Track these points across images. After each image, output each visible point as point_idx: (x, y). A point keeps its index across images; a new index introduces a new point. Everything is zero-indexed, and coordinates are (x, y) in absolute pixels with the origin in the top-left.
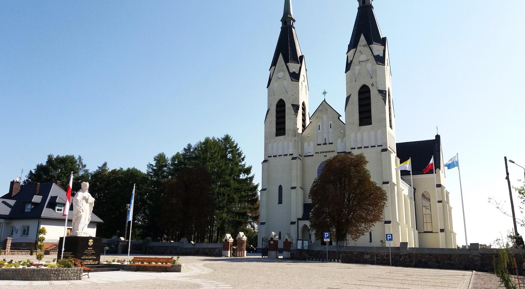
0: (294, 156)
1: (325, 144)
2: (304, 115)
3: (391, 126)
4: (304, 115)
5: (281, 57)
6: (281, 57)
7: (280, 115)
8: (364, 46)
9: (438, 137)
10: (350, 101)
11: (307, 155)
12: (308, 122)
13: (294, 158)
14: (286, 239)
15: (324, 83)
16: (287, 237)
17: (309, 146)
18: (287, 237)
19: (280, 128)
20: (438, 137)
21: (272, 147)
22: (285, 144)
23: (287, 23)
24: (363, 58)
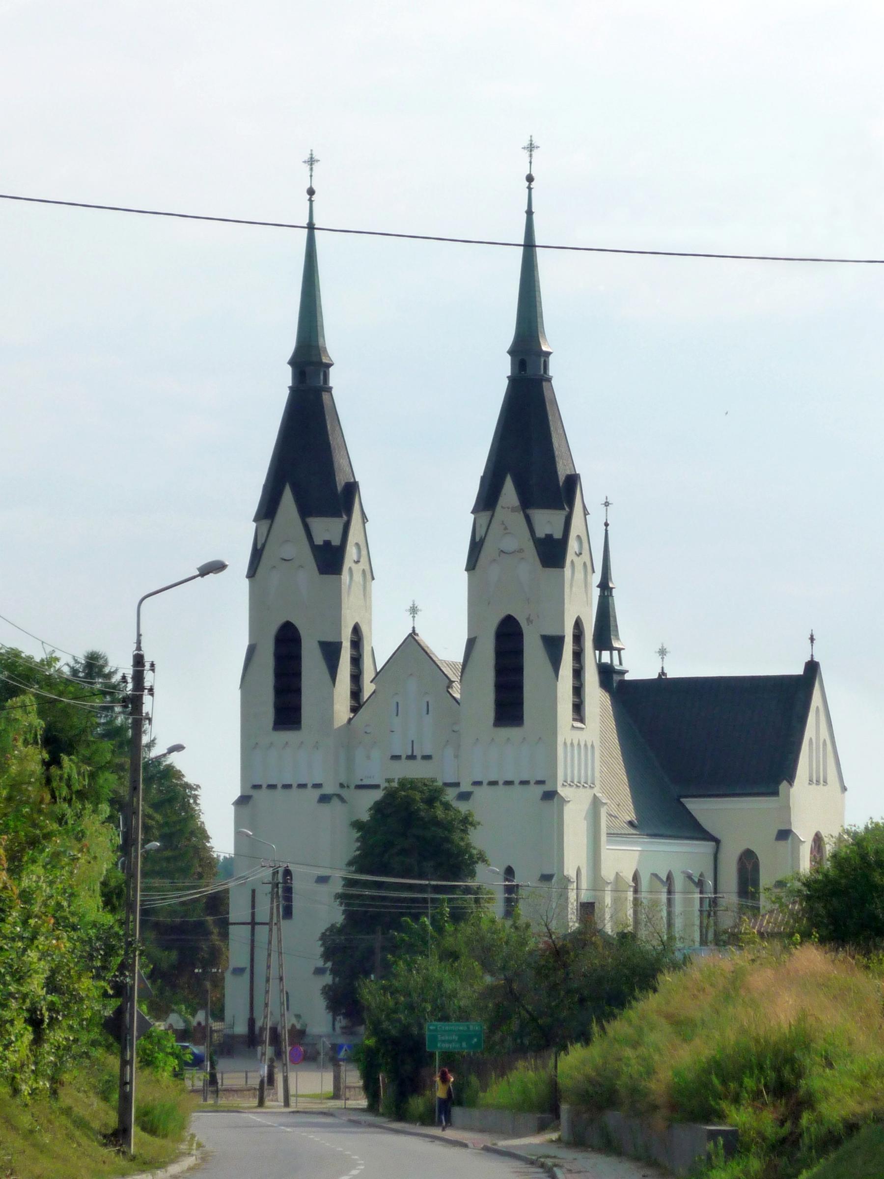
0: (328, 790)
1: (412, 757)
2: (356, 678)
3: (578, 709)
4: (356, 678)
5: (288, 498)
6: (288, 498)
7: (287, 671)
8: (513, 510)
9: (812, 667)
10: (475, 654)
11: (364, 783)
12: (368, 688)
13: (324, 799)
14: (293, 1026)
15: (415, 588)
16: (294, 1021)
17: (368, 757)
18: (294, 1021)
19: (287, 710)
20: (812, 667)
21: (443, 1041)
22: (302, 757)
23: (309, 367)
24: (509, 544)
